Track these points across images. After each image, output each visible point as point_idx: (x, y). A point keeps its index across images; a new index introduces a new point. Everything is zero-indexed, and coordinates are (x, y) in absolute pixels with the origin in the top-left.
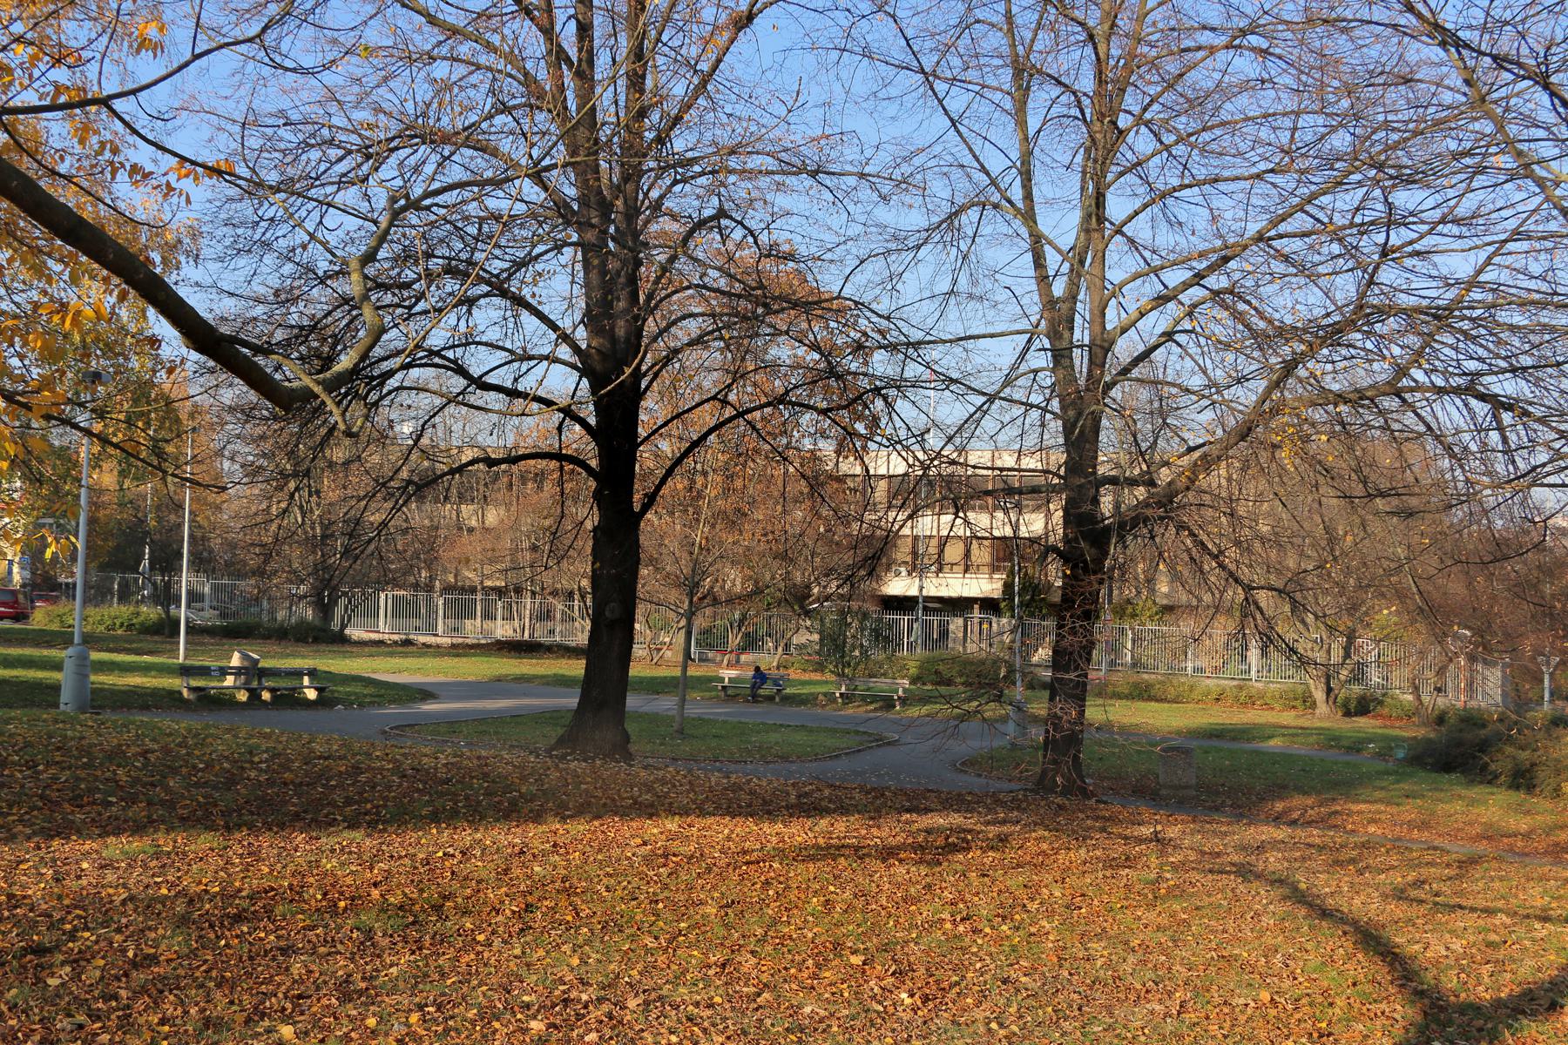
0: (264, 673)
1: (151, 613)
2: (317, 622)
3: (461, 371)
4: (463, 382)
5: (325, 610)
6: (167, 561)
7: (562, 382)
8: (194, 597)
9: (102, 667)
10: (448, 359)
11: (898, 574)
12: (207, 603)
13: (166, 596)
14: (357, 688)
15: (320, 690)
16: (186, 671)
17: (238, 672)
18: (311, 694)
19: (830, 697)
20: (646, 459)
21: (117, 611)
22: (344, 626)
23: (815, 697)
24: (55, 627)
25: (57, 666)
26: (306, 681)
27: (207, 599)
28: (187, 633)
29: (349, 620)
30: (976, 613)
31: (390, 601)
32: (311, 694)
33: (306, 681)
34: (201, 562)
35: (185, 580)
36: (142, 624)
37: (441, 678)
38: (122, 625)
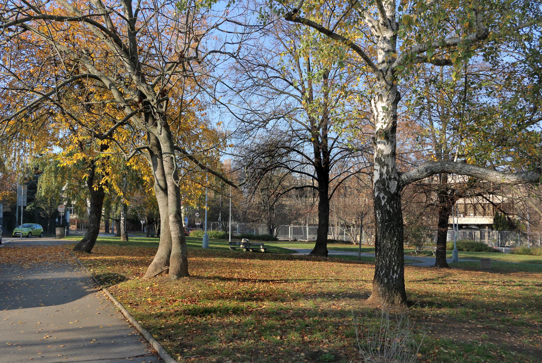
0: (250, 244)
1: (221, 232)
2: (269, 234)
3: (288, 168)
4: (288, 171)
5: (271, 231)
6: (225, 218)
7: (311, 169)
8: (234, 229)
9: (210, 243)
10: (285, 165)
11: (460, 216)
12: (237, 231)
13: (225, 229)
14: (276, 250)
15: (265, 249)
16: (231, 243)
17: (244, 244)
18: (263, 250)
19: (414, 252)
20: (331, 185)
21: (212, 232)
22: (276, 236)
23: (410, 253)
24: (196, 237)
25: (202, 243)
26: (261, 247)
27: (238, 230)
28: (231, 238)
29: (278, 234)
30: (487, 229)
31: (292, 229)
32: (263, 250)
33: (261, 247)
34: (235, 218)
35: (230, 223)
36: (219, 236)
37: (301, 248)
38: (214, 236)
